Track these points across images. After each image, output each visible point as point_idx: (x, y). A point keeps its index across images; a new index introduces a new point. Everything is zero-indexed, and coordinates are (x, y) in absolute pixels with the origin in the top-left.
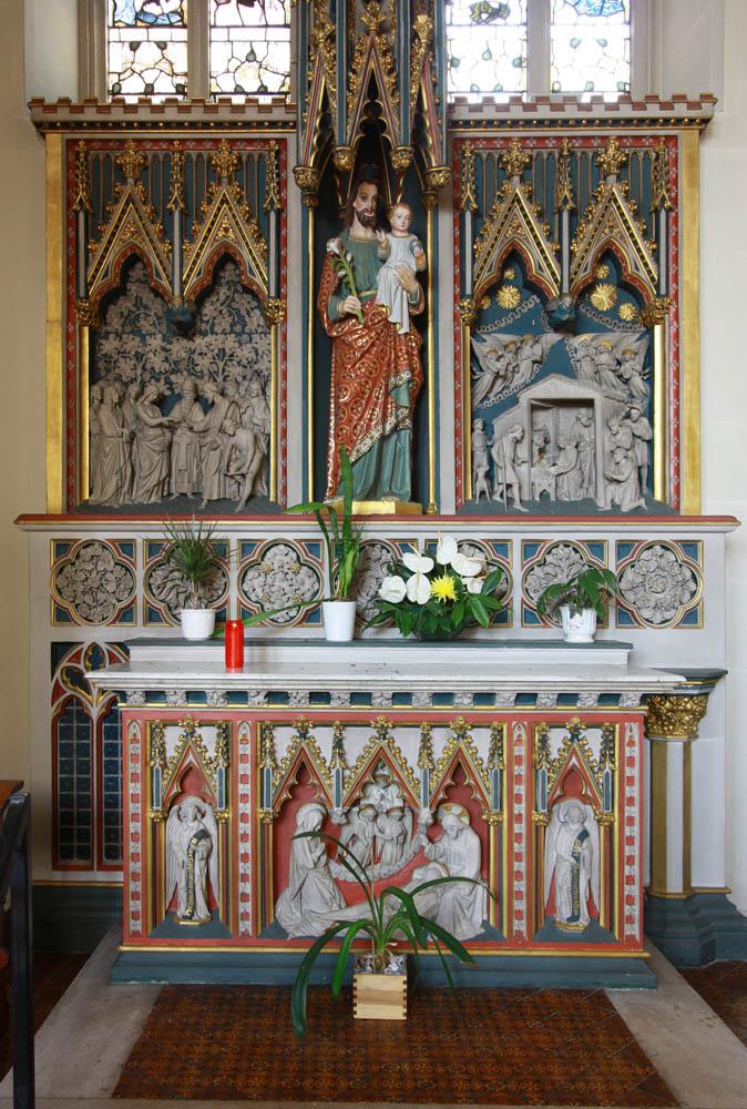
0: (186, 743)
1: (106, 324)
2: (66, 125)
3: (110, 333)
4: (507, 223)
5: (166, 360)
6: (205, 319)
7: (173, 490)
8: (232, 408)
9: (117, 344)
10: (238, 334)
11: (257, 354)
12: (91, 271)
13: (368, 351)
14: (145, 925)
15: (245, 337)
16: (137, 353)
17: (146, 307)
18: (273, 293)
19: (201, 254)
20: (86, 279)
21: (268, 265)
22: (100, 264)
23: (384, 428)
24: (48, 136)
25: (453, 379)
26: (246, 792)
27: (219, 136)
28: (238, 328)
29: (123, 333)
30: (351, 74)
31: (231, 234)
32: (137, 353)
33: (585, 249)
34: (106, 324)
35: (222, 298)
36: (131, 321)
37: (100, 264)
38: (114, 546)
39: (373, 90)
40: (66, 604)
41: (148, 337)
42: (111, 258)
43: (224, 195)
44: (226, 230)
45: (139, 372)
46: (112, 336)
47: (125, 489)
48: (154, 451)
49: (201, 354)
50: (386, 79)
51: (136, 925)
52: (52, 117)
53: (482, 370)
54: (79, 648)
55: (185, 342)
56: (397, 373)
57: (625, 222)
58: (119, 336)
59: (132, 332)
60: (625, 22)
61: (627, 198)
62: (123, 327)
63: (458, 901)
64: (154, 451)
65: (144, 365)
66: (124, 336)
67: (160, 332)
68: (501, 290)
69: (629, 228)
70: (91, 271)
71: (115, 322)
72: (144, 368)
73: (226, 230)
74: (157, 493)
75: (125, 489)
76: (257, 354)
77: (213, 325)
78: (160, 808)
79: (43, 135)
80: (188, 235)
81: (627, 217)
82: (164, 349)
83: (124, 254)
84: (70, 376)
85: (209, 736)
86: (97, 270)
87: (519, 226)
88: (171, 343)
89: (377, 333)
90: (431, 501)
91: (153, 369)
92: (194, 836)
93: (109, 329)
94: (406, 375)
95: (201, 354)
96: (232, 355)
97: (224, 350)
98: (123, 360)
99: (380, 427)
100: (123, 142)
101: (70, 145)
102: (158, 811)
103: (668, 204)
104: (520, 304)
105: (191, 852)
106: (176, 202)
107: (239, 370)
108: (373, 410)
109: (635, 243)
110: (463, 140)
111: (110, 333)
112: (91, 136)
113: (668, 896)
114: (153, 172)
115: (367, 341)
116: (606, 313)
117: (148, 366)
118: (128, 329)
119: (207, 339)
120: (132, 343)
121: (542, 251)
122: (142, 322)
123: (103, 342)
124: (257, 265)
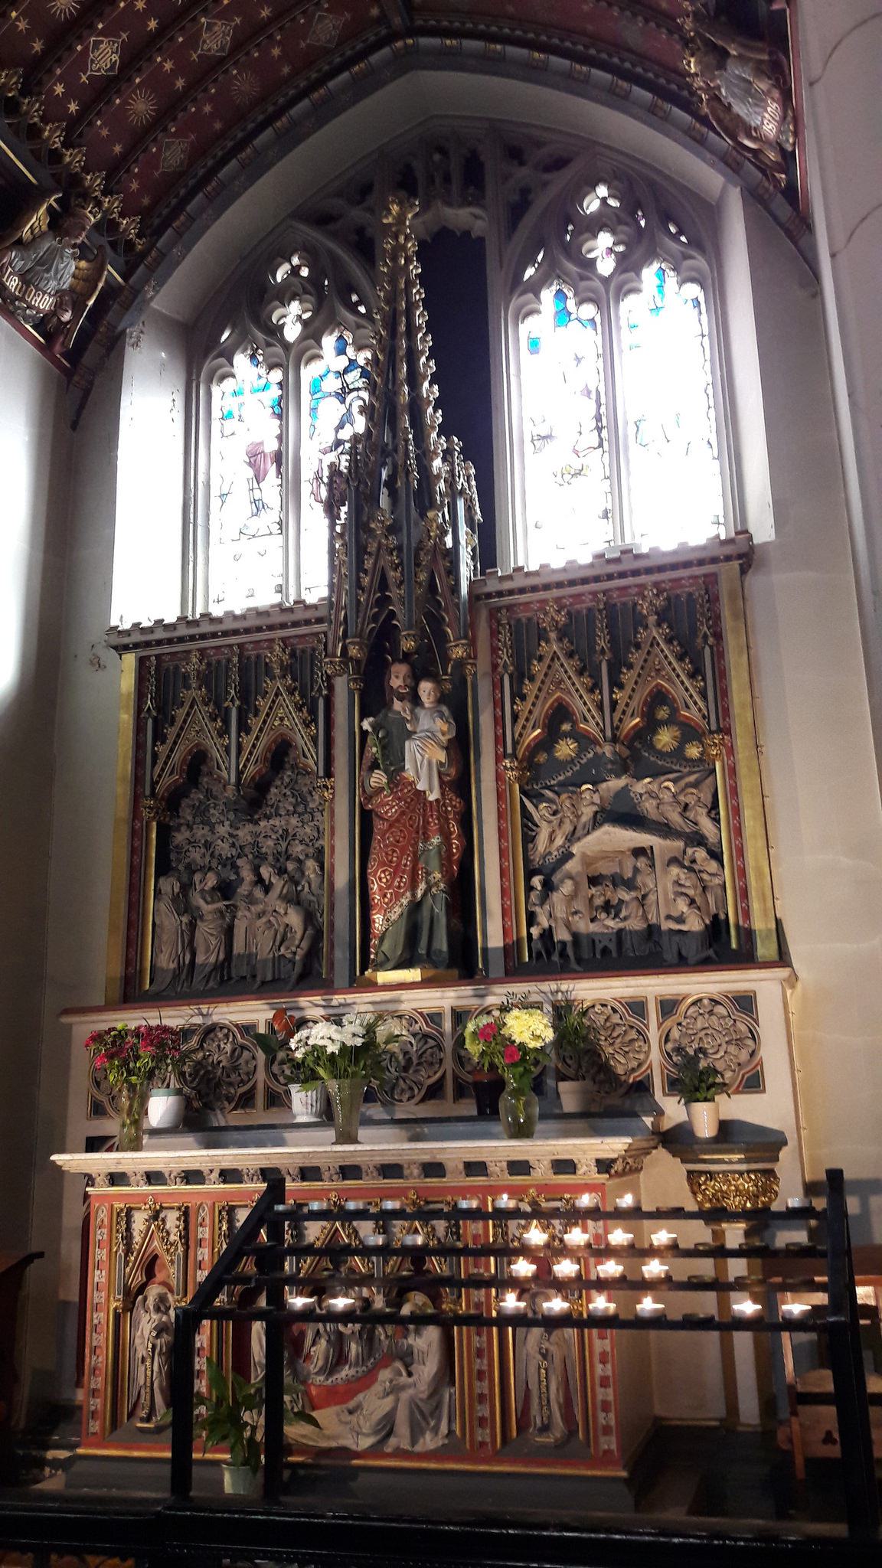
0: (149, 1228)
1: (179, 817)
2: (136, 646)
3: (182, 824)
4: (548, 681)
5: (233, 845)
6: (270, 803)
7: (233, 975)
8: (286, 886)
9: (187, 834)
10: (300, 815)
11: (318, 832)
12: (157, 770)
13: (397, 820)
14: (103, 1428)
15: (307, 817)
16: (206, 841)
17: (216, 798)
18: (321, 773)
19: (258, 743)
20: (152, 778)
21: (316, 745)
22: (166, 763)
23: (414, 895)
24: (123, 657)
25: (497, 836)
26: (603, 1390)
27: (272, 636)
28: (301, 809)
29: (194, 823)
30: (362, 575)
31: (286, 722)
32: (206, 841)
33: (632, 697)
34: (179, 817)
35: (287, 780)
36: (201, 812)
37: (166, 763)
38: (647, 1069)
39: (384, 584)
40: (103, 1098)
41: (217, 826)
42: (177, 757)
43: (278, 688)
44: (282, 719)
45: (208, 858)
46: (183, 828)
47: (183, 976)
48: (212, 935)
49: (265, 837)
50: (392, 573)
51: (95, 1426)
52: (126, 640)
53: (537, 826)
54: (112, 1143)
55: (250, 827)
56: (426, 839)
57: (670, 663)
58: (190, 827)
59: (202, 823)
60: (714, 458)
61: (669, 641)
62: (194, 818)
63: (418, 1407)
64: (212, 935)
65: (213, 852)
66: (195, 826)
67: (228, 819)
68: (557, 743)
69: (674, 670)
70: (157, 770)
71: (187, 814)
72: (212, 855)
73: (282, 719)
74: (215, 977)
75: (183, 976)
76: (318, 832)
77: (278, 808)
78: (121, 1297)
79: (120, 655)
80: (244, 728)
81: (570, 673)
82: (231, 835)
83: (274, 741)
84: (135, 872)
85: (172, 1220)
86: (163, 770)
87: (562, 681)
88: (238, 829)
89: (406, 802)
90: (480, 966)
91: (220, 855)
92: (154, 1329)
93: (182, 821)
94: (436, 840)
95: (265, 837)
96: (295, 835)
97: (287, 831)
98: (193, 850)
99: (408, 894)
100: (189, 652)
101: (142, 662)
102: (119, 1300)
103: (711, 640)
104: (578, 756)
105: (150, 1345)
106: (232, 701)
107: (300, 848)
108: (402, 877)
109: (682, 683)
110: (499, 609)
111: (182, 824)
112: (202, 646)
113: (740, 1429)
114: (212, 677)
115: (396, 811)
116: (669, 755)
117: (217, 853)
118: (198, 820)
119: (272, 822)
120: (201, 832)
121: (687, 690)
122: (212, 811)
123: (175, 834)
124: (309, 750)
